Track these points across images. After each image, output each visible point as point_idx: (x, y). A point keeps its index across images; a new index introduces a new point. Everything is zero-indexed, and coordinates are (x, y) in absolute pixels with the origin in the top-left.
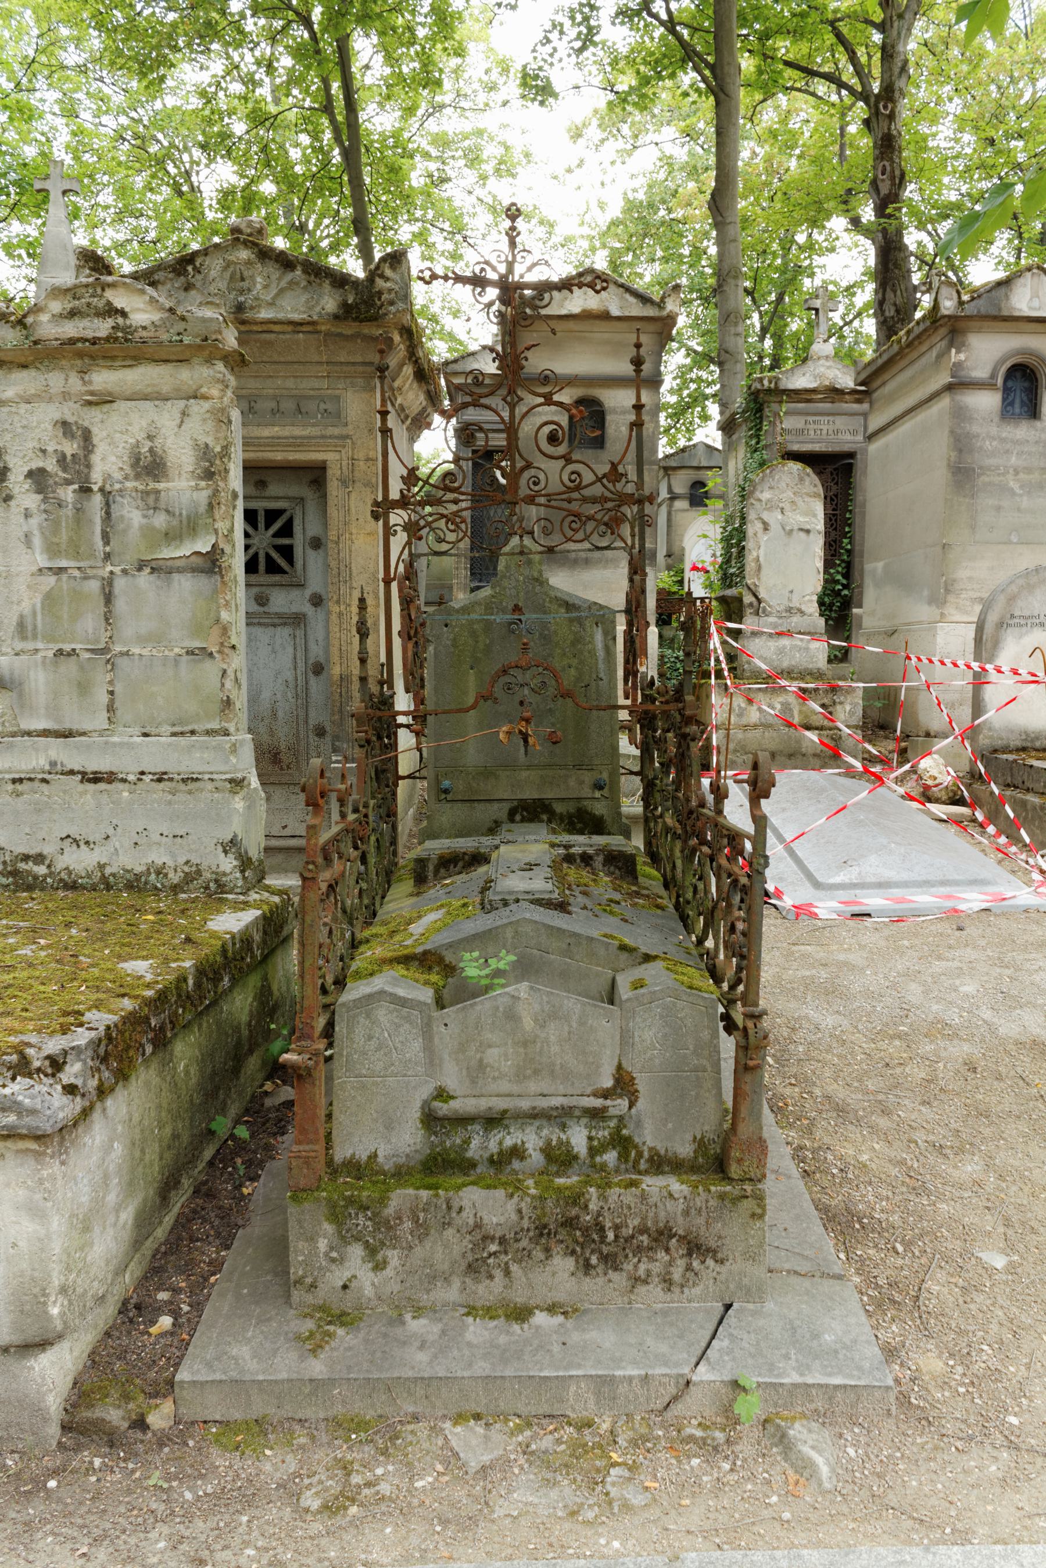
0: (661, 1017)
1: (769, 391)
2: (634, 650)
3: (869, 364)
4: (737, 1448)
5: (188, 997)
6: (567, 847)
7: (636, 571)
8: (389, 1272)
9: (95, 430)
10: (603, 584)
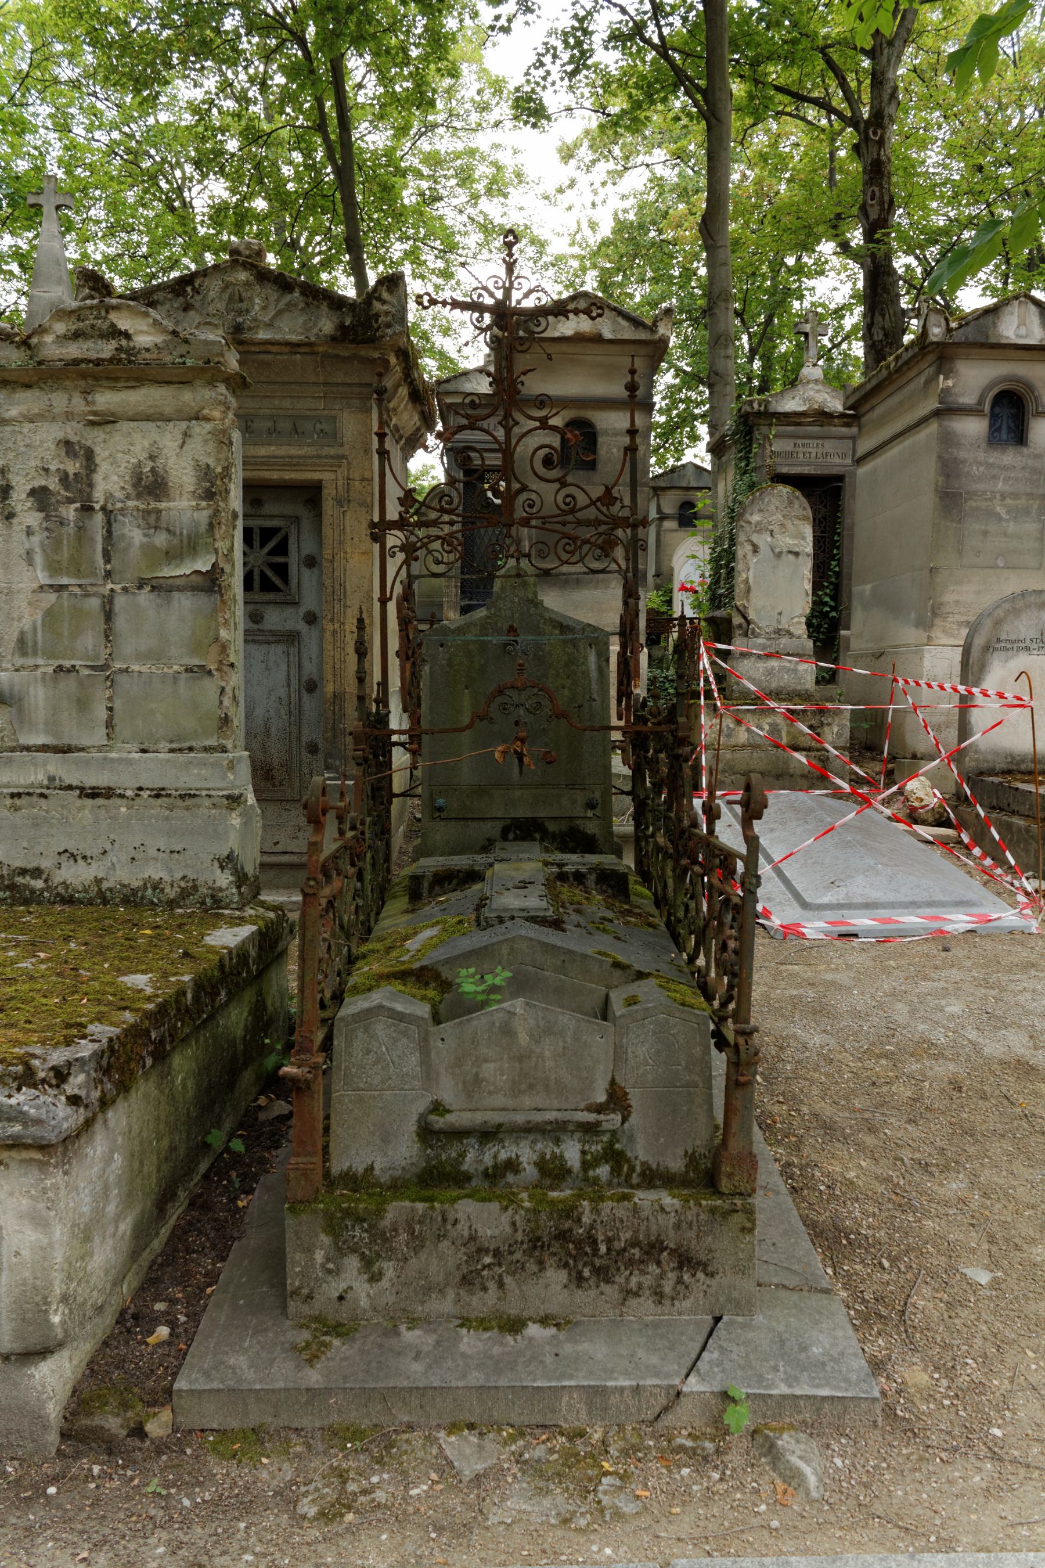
0: (654, 1033)
1: (759, 414)
2: (627, 671)
3: (858, 388)
4: (727, 1458)
5: (187, 1010)
6: (560, 865)
7: (630, 594)
8: (384, 1283)
9: (97, 450)
10: (598, 606)
